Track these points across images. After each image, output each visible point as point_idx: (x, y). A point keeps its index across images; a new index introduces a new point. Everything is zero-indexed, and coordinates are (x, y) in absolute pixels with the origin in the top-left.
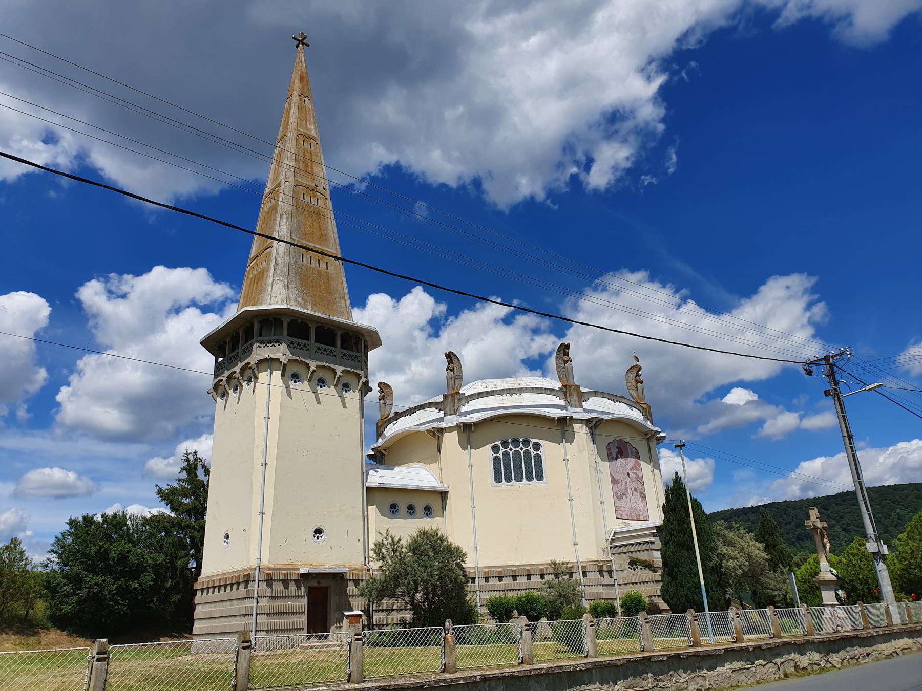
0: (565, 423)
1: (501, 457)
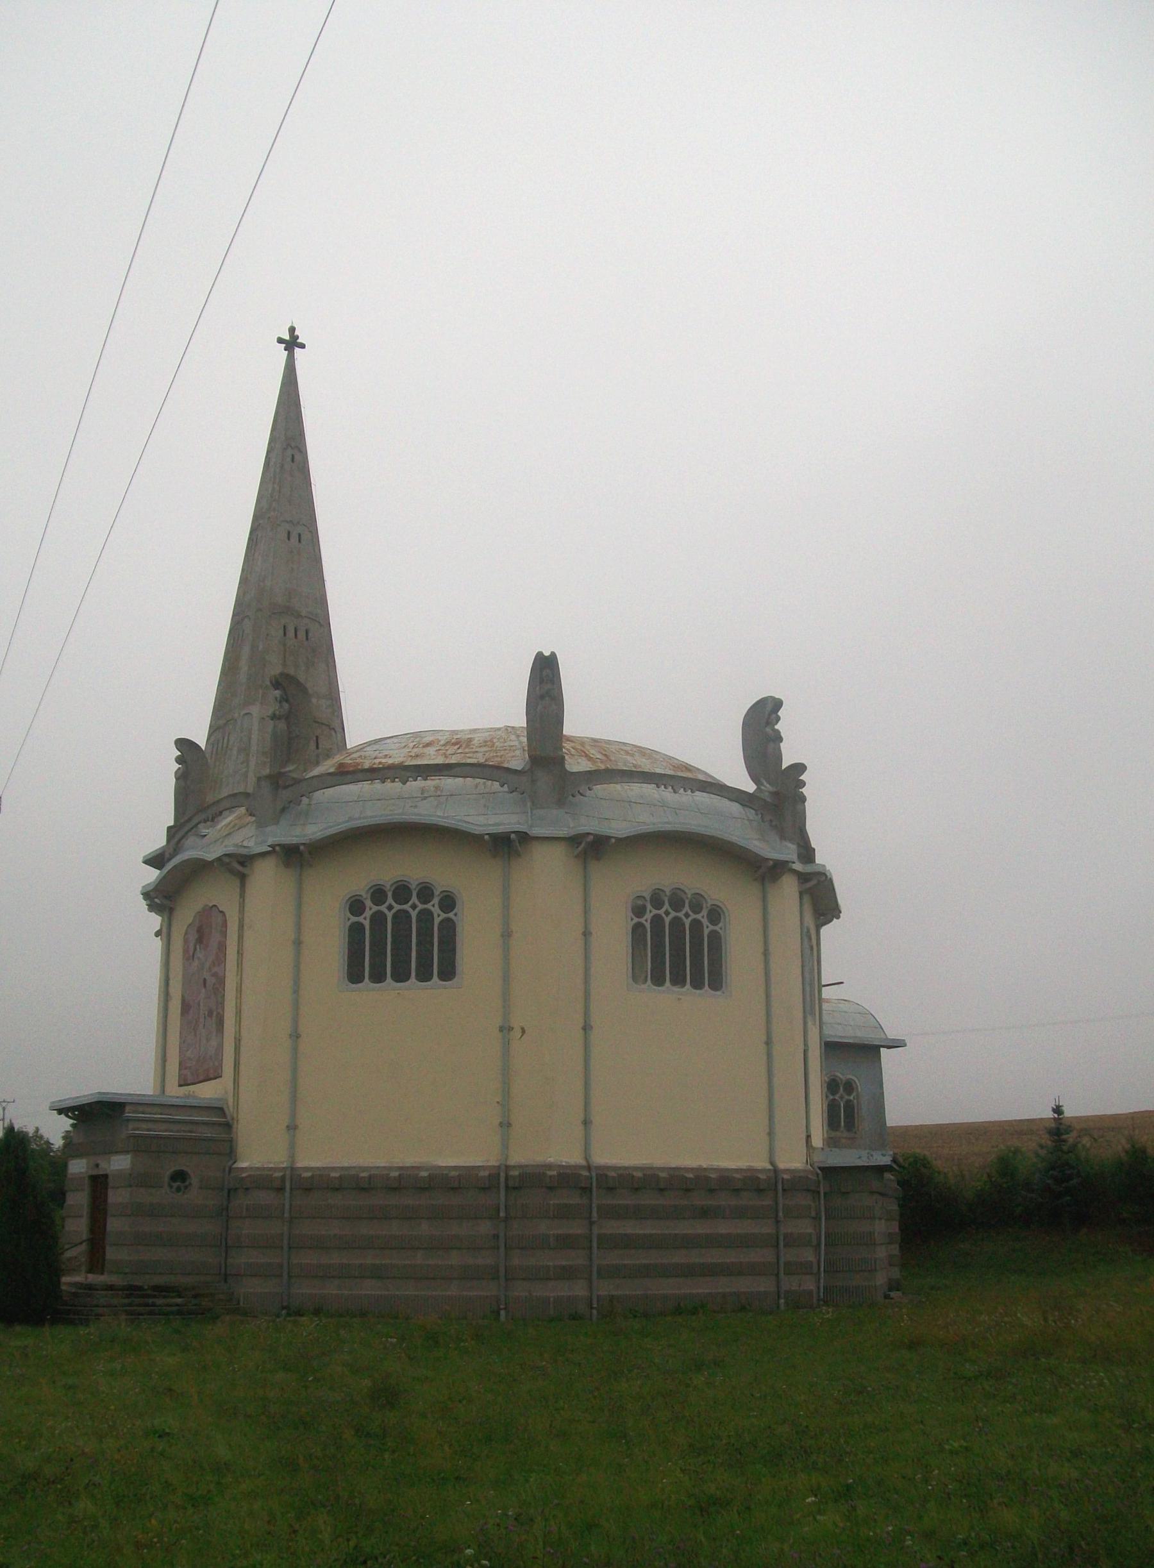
0: (506, 846)
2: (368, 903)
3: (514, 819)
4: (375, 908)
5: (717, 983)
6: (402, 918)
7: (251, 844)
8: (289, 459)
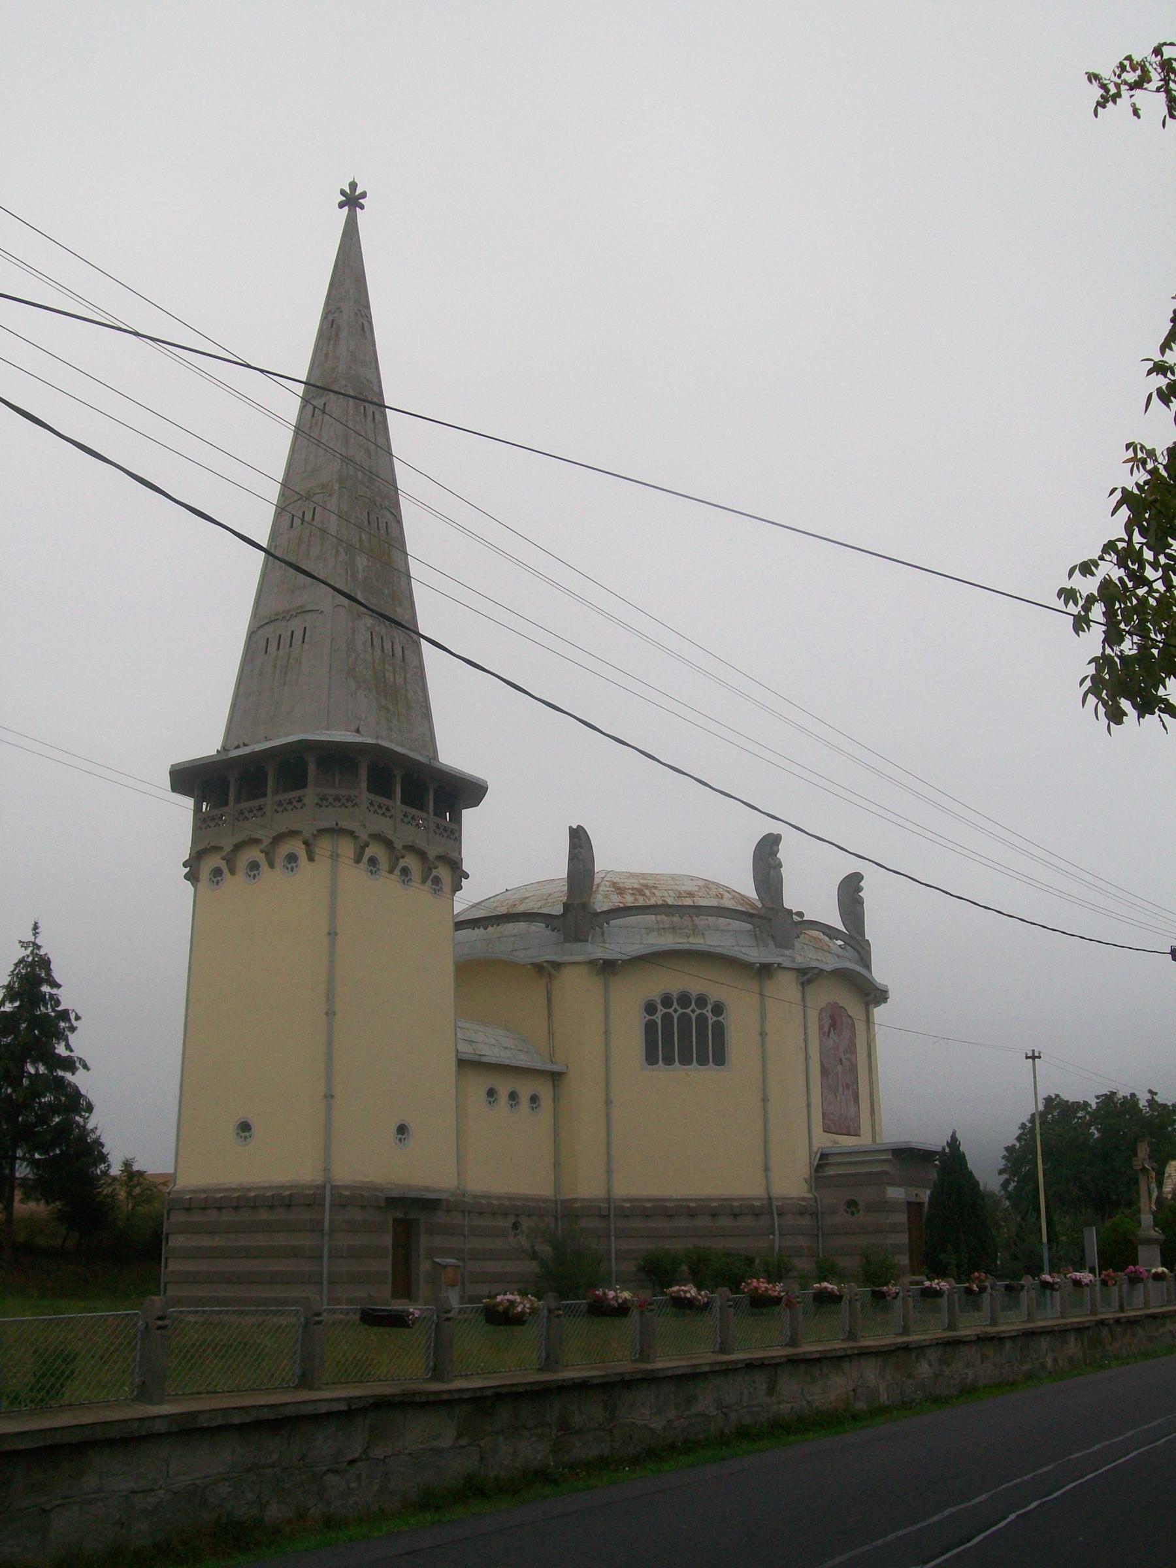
0: (765, 971)
1: (659, 1021)
2: (660, 1007)
5: (720, 1059)
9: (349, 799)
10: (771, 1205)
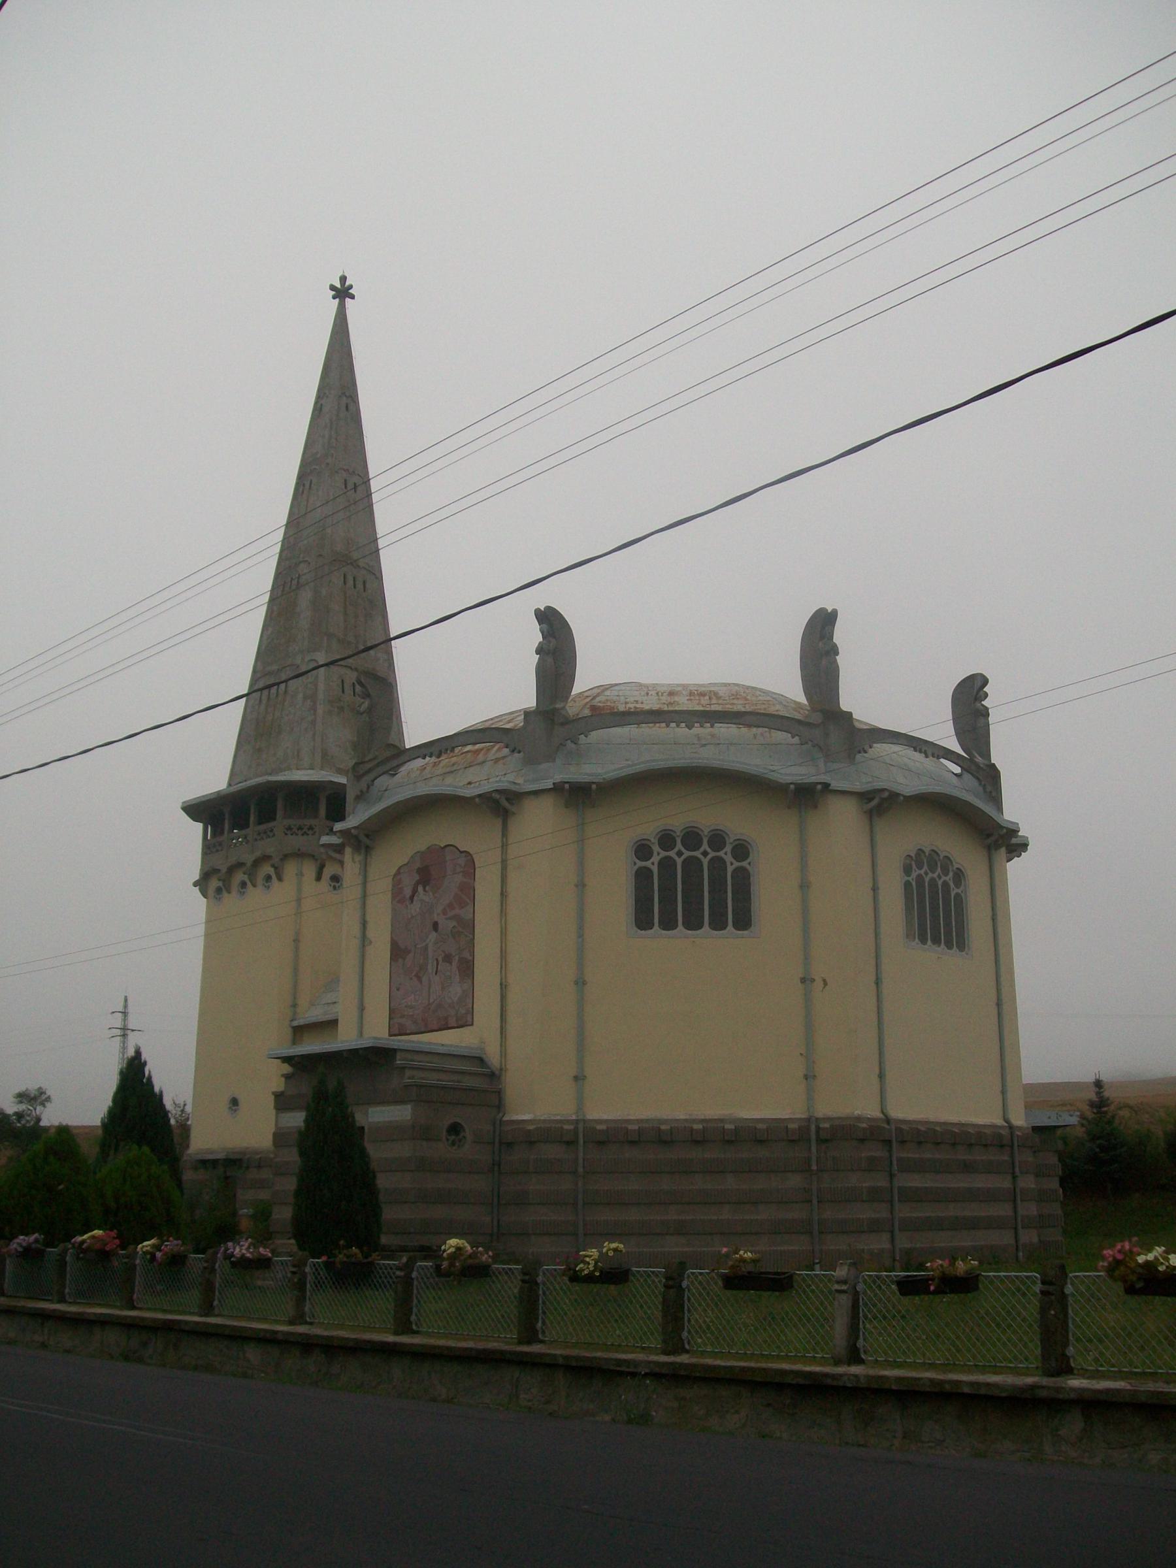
0: (806, 797)
1: (655, 869)
2: (656, 848)
3: (803, 770)
4: (664, 854)
5: (744, 921)
6: (692, 866)
7: (520, 781)
8: (344, 408)
9: (311, 828)
10: (1012, 1134)
